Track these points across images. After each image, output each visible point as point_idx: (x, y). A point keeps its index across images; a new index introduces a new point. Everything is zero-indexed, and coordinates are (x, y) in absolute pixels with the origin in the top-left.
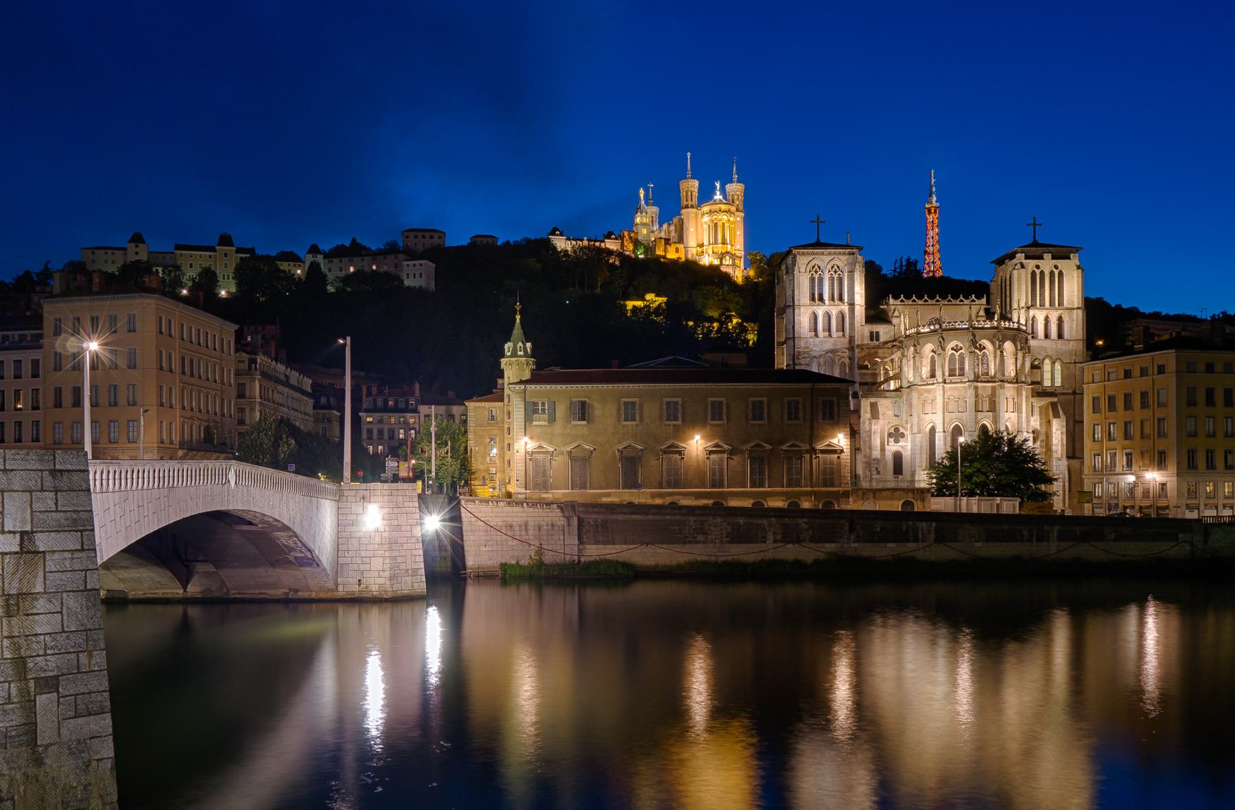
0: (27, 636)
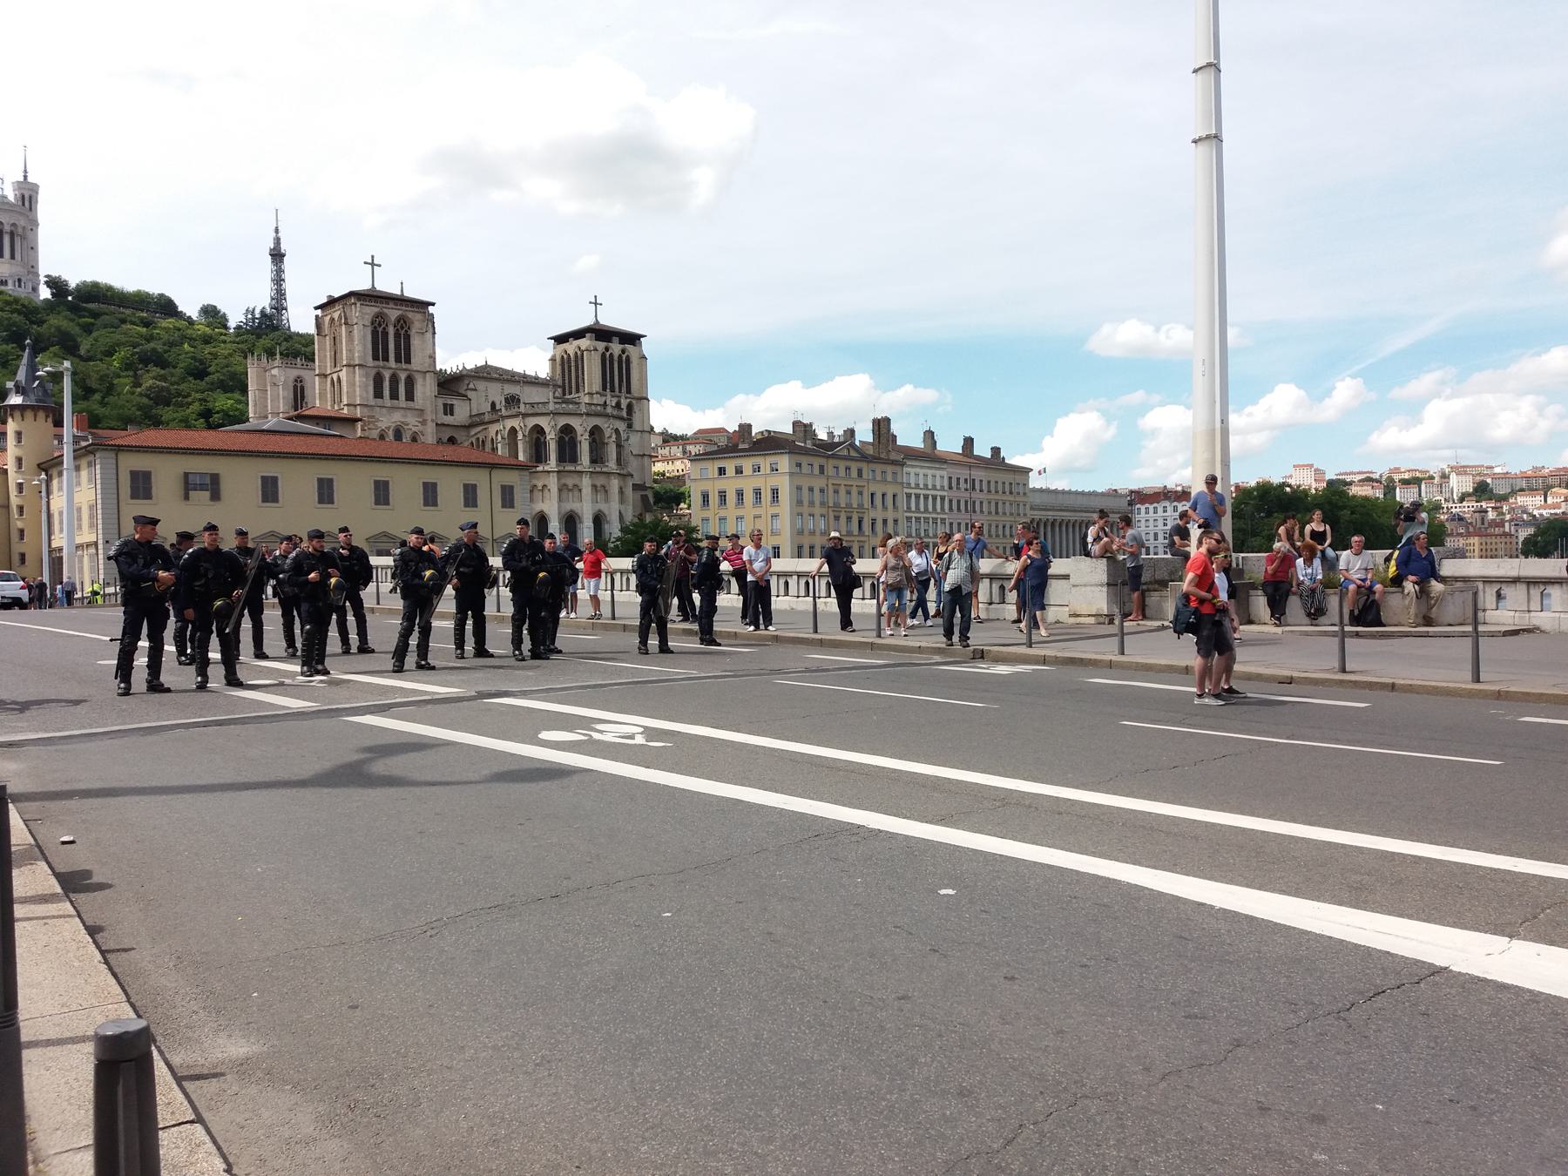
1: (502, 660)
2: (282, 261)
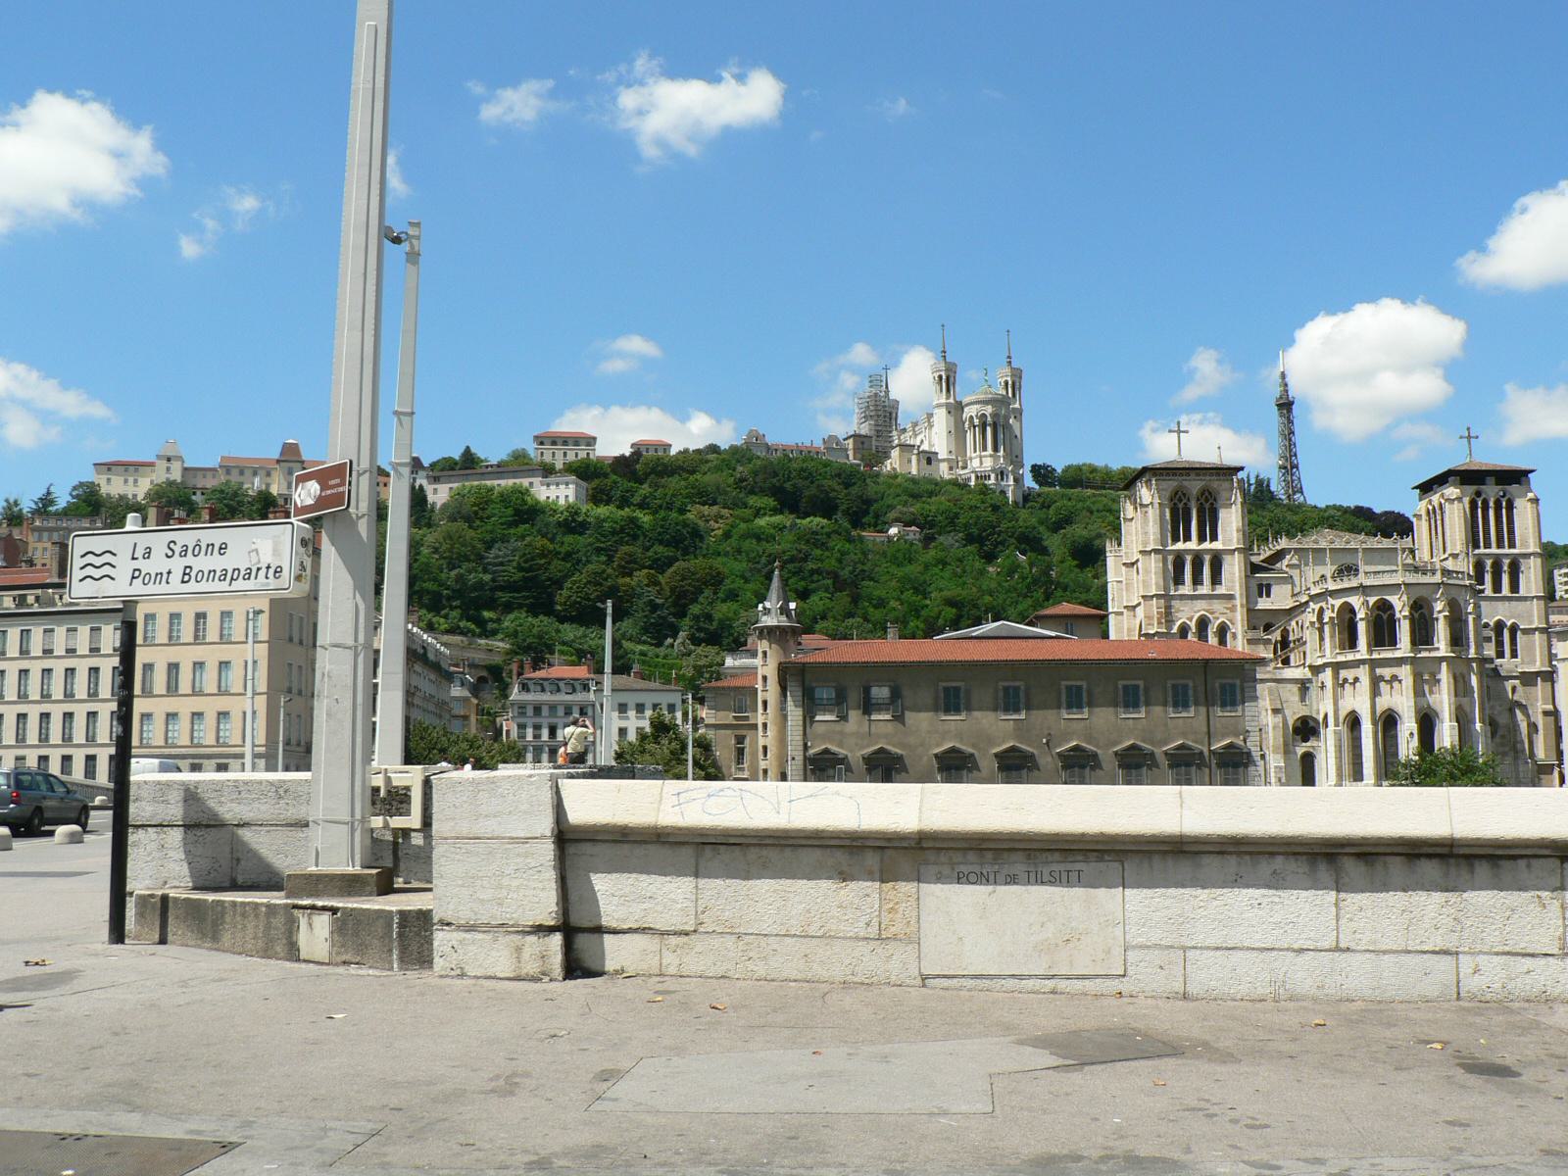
2: (1290, 411)
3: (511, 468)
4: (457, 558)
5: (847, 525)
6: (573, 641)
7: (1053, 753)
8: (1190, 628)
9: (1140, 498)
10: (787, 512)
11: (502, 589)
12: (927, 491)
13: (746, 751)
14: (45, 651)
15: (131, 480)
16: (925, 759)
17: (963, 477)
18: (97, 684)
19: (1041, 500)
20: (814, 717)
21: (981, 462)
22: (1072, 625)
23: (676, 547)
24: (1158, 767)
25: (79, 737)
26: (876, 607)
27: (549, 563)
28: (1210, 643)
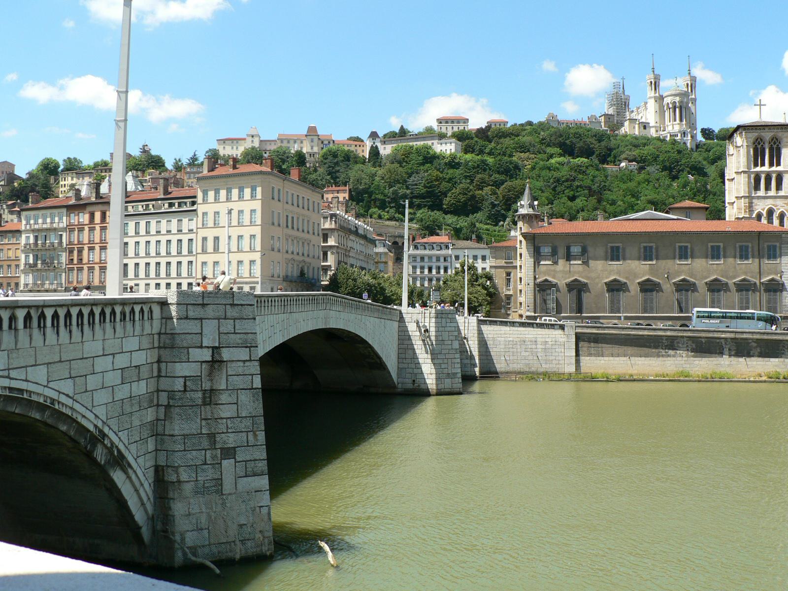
0: (216, 419)
1: (778, 335)
3: (424, 136)
4: (394, 182)
5: (597, 162)
6: (452, 223)
7: (671, 282)
8: (763, 215)
9: (736, 142)
10: (567, 156)
11: (416, 197)
12: (642, 143)
13: (512, 280)
14: (157, 232)
15: (235, 147)
16: (600, 285)
17: (663, 135)
18: (181, 248)
19: (705, 147)
20: (540, 262)
21: (673, 127)
22: (689, 212)
23: (507, 175)
24: (730, 291)
25: (174, 274)
26: (611, 205)
27: (440, 184)
28: (762, 222)
